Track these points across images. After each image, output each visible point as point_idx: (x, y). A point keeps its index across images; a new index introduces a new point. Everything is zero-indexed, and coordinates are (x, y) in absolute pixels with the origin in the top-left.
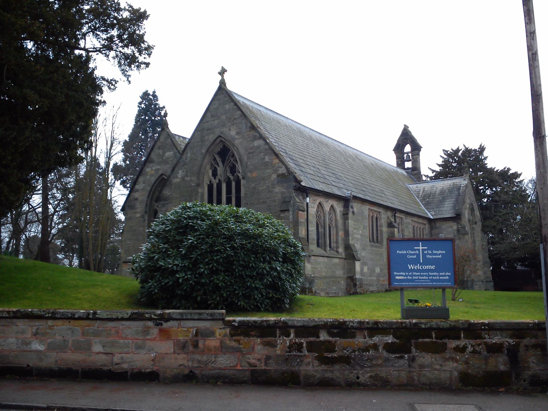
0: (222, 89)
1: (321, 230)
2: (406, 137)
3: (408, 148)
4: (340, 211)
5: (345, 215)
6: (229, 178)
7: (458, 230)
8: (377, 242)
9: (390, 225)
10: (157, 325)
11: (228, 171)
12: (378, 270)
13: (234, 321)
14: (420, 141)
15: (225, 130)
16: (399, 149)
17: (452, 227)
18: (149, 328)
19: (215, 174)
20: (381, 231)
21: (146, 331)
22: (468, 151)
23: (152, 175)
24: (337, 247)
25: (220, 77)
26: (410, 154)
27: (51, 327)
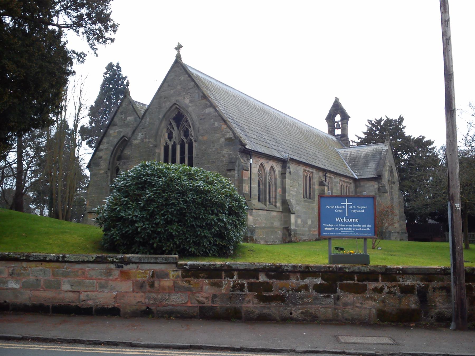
0: (178, 62)
1: (261, 187)
2: (337, 108)
3: (338, 118)
4: (279, 171)
5: (283, 175)
6: (183, 141)
7: (379, 189)
8: (310, 198)
9: (321, 184)
10: (118, 267)
11: (182, 134)
12: (309, 222)
13: (186, 265)
14: (348, 112)
15: (180, 98)
16: (330, 118)
17: (373, 186)
18: (111, 270)
19: (170, 137)
20: (314, 189)
21: (109, 273)
22: (389, 122)
23: (114, 137)
24: (276, 202)
25: (176, 52)
26: (340, 123)
27: (25, 269)
